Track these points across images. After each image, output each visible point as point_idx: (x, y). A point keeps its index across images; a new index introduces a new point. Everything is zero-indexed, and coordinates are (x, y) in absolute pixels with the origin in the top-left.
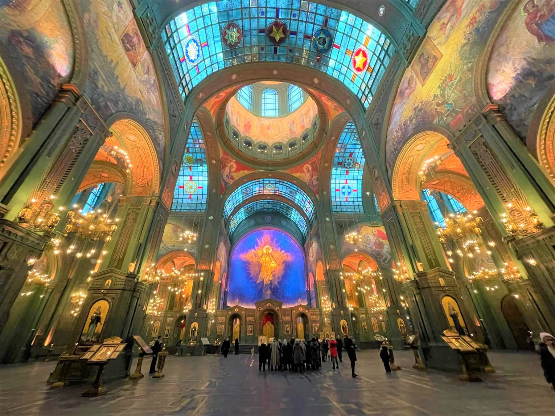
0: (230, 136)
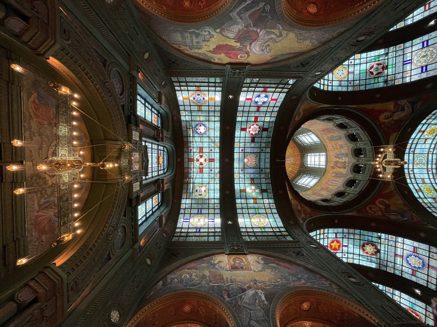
0: (340, 201)
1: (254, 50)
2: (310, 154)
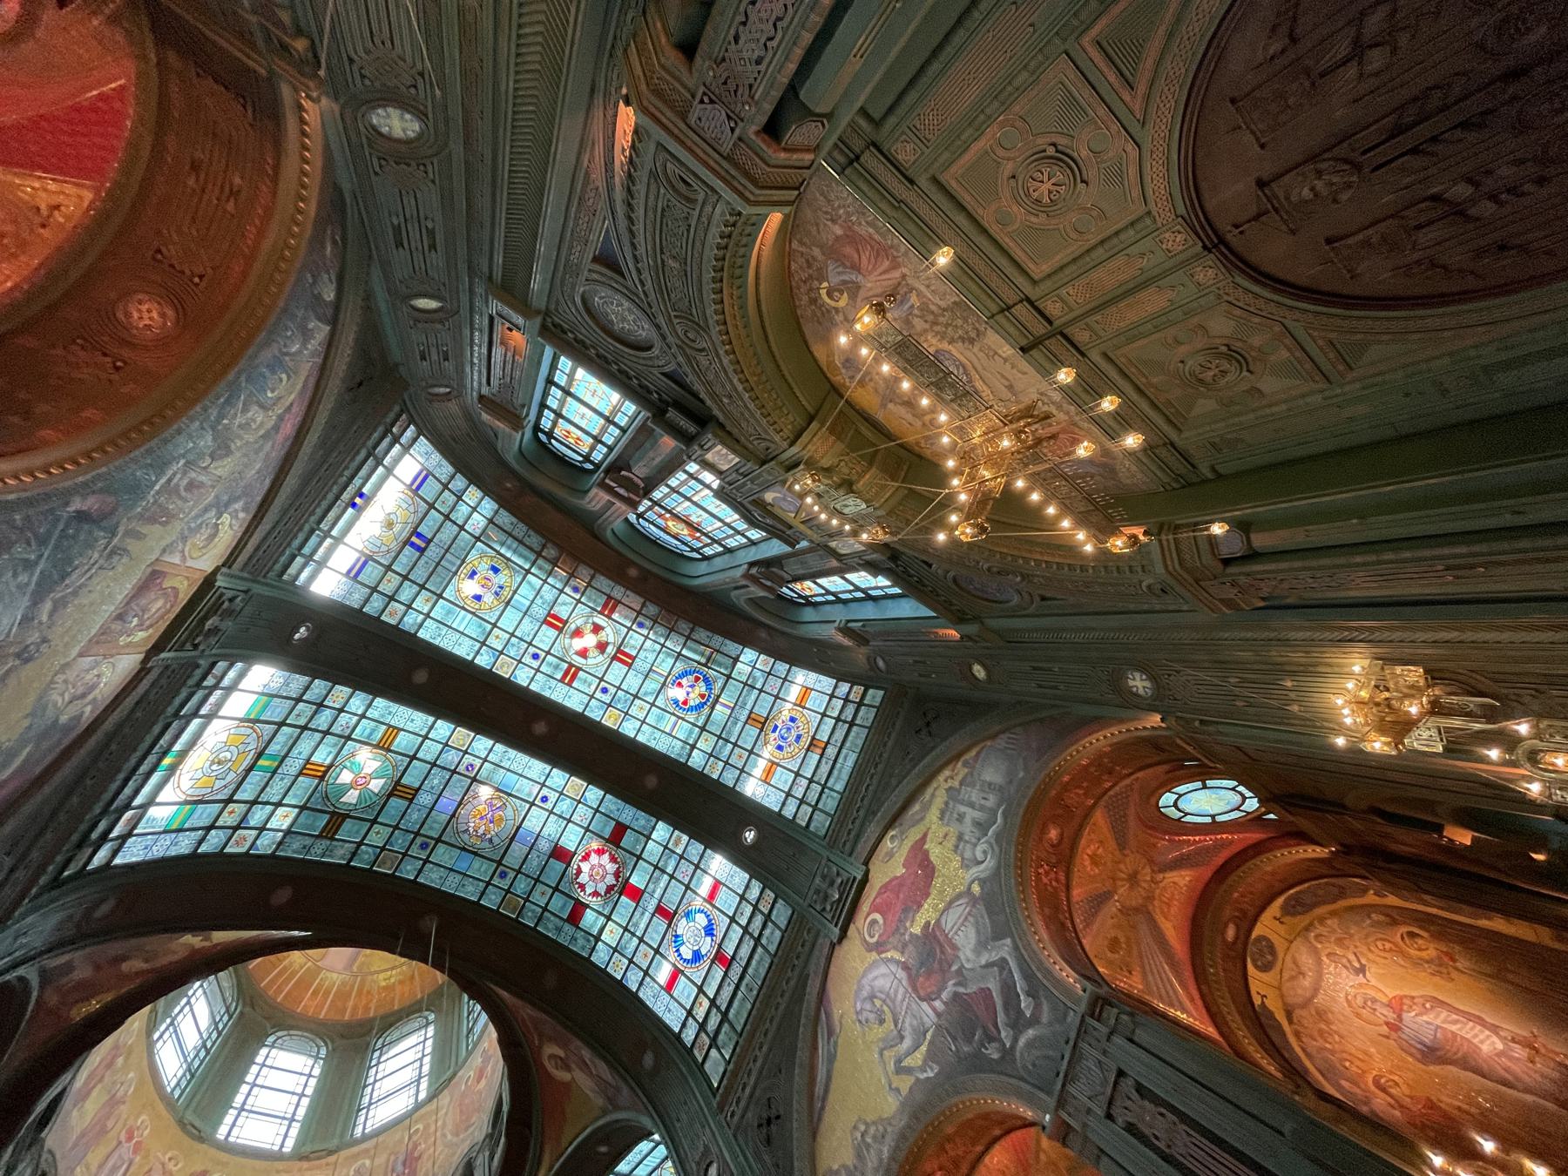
1: (883, 969)
2: (317, 1071)
